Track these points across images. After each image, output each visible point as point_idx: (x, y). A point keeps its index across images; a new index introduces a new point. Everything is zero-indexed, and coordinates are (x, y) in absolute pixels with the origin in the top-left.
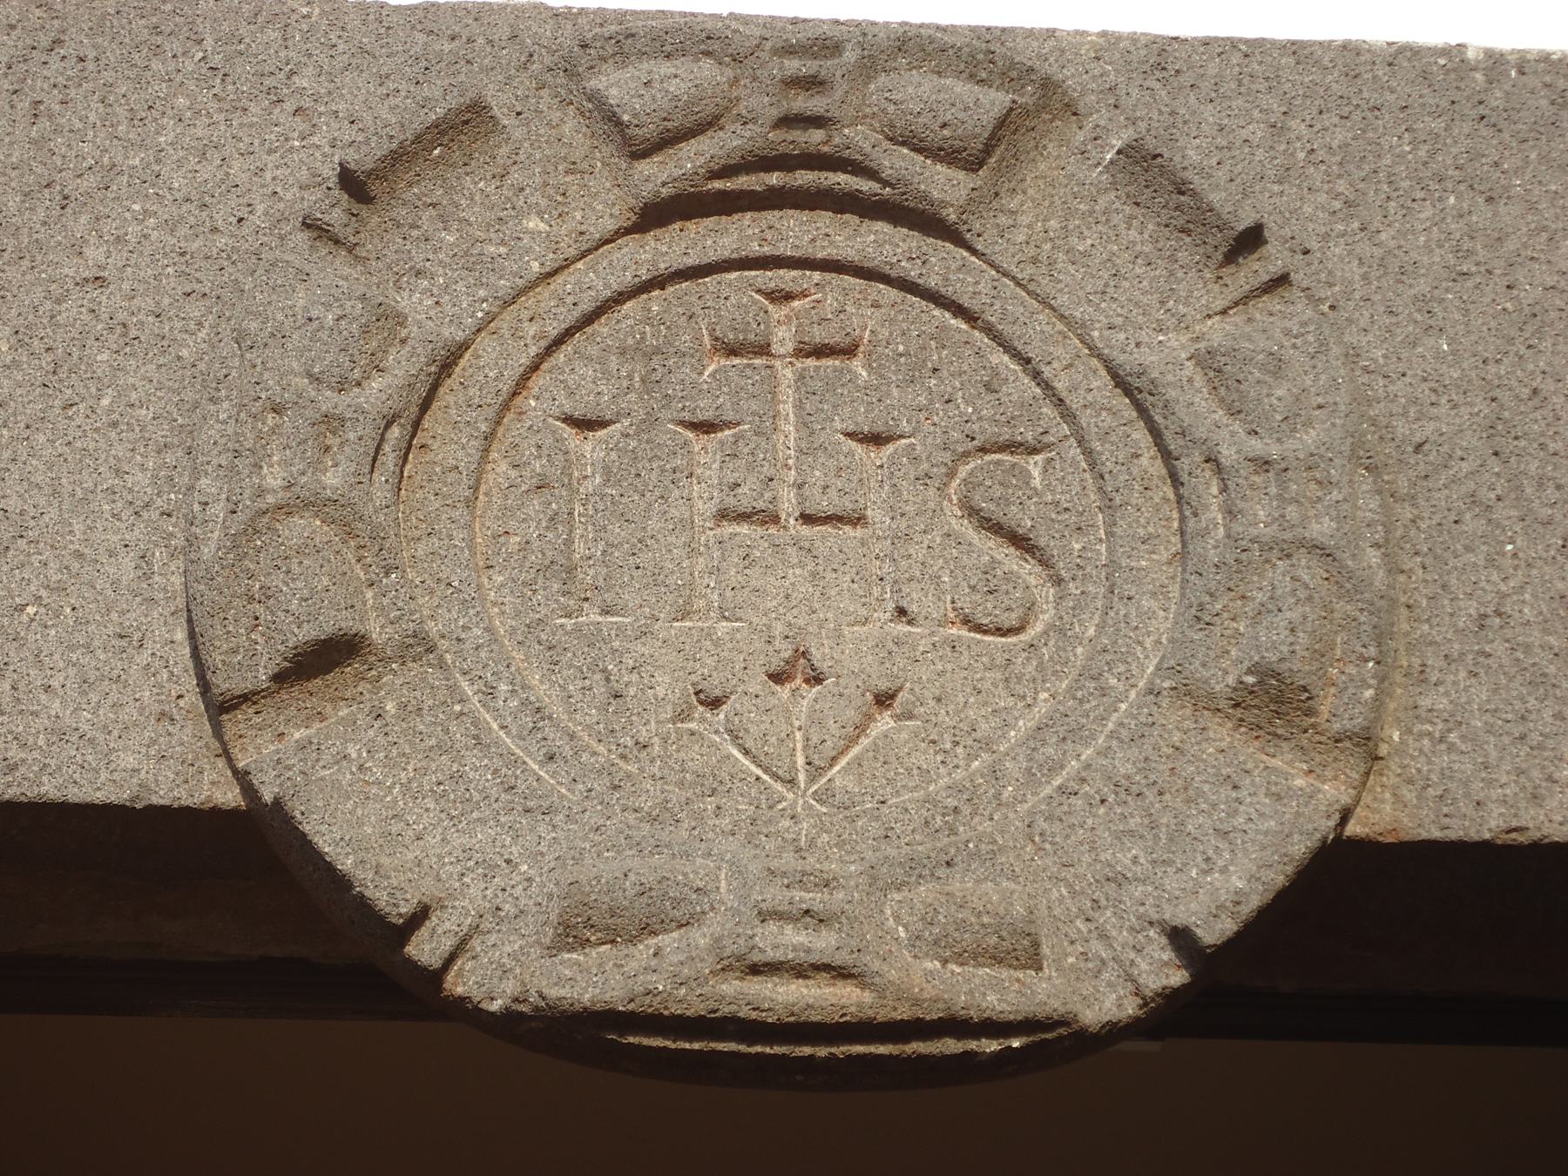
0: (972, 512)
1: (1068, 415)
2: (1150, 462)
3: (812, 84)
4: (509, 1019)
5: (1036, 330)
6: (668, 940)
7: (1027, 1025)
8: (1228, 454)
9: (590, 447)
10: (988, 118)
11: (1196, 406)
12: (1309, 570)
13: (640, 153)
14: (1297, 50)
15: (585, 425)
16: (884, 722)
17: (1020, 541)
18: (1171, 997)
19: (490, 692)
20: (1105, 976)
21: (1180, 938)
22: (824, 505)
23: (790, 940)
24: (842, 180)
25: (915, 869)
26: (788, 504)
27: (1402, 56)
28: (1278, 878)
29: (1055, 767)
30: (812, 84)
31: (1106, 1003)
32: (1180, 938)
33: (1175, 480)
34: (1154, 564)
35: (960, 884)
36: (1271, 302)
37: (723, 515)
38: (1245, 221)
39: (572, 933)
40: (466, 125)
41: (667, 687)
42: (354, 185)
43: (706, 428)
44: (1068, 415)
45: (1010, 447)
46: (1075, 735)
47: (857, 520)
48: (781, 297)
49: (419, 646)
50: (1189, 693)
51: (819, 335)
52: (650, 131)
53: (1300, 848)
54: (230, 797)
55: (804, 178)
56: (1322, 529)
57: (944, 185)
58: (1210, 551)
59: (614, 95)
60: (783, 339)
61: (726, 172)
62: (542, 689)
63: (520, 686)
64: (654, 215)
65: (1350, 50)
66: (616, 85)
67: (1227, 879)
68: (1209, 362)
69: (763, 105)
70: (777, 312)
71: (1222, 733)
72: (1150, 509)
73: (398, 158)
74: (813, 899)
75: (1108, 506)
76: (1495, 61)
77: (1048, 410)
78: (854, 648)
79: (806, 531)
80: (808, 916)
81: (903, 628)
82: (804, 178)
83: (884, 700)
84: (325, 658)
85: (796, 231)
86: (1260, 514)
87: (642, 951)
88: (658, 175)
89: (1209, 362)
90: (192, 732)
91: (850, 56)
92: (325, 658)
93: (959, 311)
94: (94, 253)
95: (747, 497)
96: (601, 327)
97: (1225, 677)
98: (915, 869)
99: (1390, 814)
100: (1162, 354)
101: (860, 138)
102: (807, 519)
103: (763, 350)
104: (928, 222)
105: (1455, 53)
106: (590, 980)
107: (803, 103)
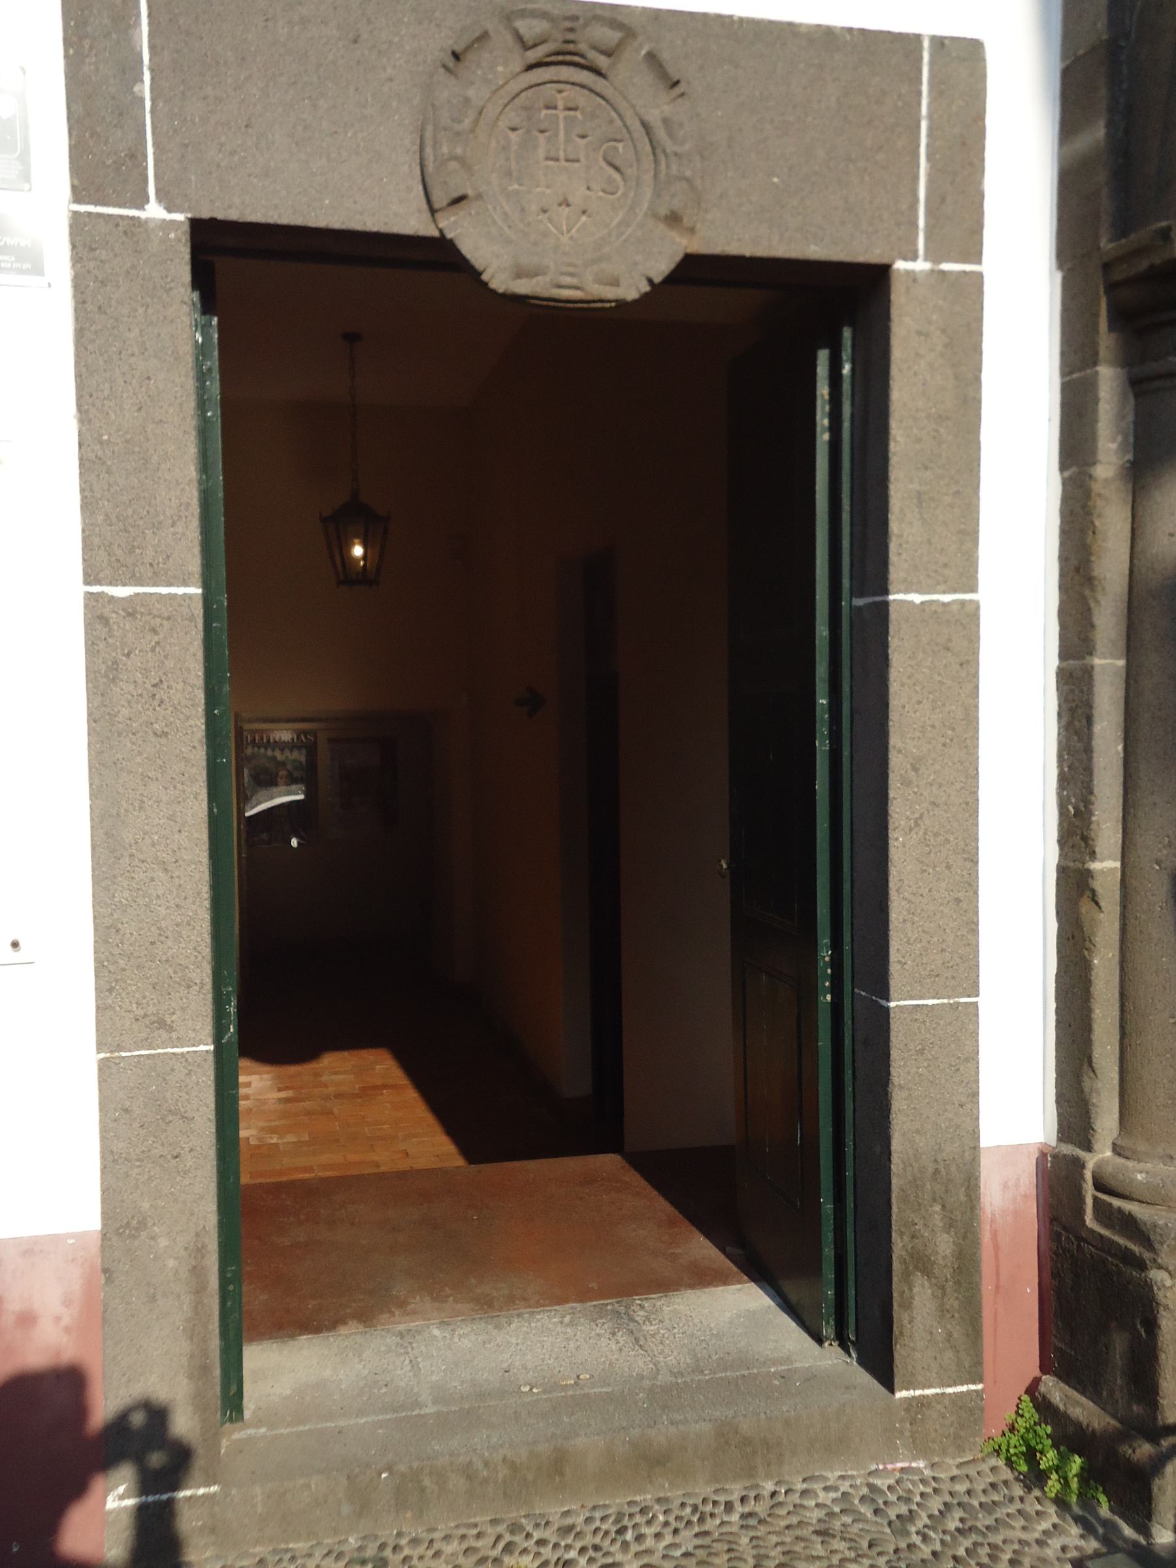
0: (605, 159)
1: (629, 132)
2: (648, 148)
3: (571, 30)
4: (504, 296)
5: (623, 106)
6: (540, 278)
7: (616, 301)
8: (668, 151)
9: (513, 136)
10: (616, 42)
11: (661, 134)
12: (684, 185)
13: (526, 47)
14: (691, 15)
15: (514, 129)
16: (584, 218)
17: (617, 169)
18: (646, 294)
19: (495, 208)
20: (631, 289)
21: (650, 281)
22: (571, 157)
23: (567, 280)
24: (577, 59)
25: (594, 262)
26: (562, 155)
27: (719, 17)
28: (672, 266)
29: (623, 233)
30: (571, 30)
31: (631, 295)
32: (650, 281)
33: (654, 154)
34: (648, 178)
35: (604, 265)
36: (680, 100)
37: (547, 159)
38: (675, 79)
39: (519, 274)
40: (484, 36)
41: (534, 208)
42: (456, 56)
43: (542, 132)
44: (629, 132)
45: (615, 140)
46: (628, 225)
47: (578, 161)
48: (560, 92)
49: (479, 196)
50: (655, 216)
51: (570, 105)
52: (531, 43)
53: (678, 258)
54: (436, 234)
55: (568, 58)
56: (688, 173)
57: (602, 61)
58: (662, 176)
59: (522, 31)
60: (561, 104)
61: (549, 56)
62: (507, 208)
63: (502, 207)
64: (530, 67)
65: (705, 15)
66: (521, 25)
67: (661, 268)
68: (665, 121)
69: (560, 37)
70: (559, 96)
71: (662, 226)
72: (648, 162)
73: (468, 48)
74: (571, 269)
75: (638, 160)
76: (741, 20)
77: (625, 131)
78: (578, 194)
79: (567, 164)
80: (572, 275)
81: (588, 192)
82: (568, 58)
83: (584, 212)
84: (459, 200)
85: (566, 73)
86: (674, 168)
87: (535, 280)
88: (533, 55)
89: (665, 121)
90: (426, 215)
91: (581, 21)
92: (459, 200)
93: (603, 97)
94: (389, 70)
95: (552, 154)
96: (516, 100)
97: (663, 211)
98: (594, 262)
99: (698, 246)
100: (654, 116)
101: (582, 47)
102: (567, 160)
103: (555, 108)
104: (597, 72)
105: (731, 17)
106: (522, 287)
107: (570, 36)
